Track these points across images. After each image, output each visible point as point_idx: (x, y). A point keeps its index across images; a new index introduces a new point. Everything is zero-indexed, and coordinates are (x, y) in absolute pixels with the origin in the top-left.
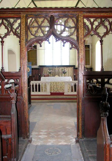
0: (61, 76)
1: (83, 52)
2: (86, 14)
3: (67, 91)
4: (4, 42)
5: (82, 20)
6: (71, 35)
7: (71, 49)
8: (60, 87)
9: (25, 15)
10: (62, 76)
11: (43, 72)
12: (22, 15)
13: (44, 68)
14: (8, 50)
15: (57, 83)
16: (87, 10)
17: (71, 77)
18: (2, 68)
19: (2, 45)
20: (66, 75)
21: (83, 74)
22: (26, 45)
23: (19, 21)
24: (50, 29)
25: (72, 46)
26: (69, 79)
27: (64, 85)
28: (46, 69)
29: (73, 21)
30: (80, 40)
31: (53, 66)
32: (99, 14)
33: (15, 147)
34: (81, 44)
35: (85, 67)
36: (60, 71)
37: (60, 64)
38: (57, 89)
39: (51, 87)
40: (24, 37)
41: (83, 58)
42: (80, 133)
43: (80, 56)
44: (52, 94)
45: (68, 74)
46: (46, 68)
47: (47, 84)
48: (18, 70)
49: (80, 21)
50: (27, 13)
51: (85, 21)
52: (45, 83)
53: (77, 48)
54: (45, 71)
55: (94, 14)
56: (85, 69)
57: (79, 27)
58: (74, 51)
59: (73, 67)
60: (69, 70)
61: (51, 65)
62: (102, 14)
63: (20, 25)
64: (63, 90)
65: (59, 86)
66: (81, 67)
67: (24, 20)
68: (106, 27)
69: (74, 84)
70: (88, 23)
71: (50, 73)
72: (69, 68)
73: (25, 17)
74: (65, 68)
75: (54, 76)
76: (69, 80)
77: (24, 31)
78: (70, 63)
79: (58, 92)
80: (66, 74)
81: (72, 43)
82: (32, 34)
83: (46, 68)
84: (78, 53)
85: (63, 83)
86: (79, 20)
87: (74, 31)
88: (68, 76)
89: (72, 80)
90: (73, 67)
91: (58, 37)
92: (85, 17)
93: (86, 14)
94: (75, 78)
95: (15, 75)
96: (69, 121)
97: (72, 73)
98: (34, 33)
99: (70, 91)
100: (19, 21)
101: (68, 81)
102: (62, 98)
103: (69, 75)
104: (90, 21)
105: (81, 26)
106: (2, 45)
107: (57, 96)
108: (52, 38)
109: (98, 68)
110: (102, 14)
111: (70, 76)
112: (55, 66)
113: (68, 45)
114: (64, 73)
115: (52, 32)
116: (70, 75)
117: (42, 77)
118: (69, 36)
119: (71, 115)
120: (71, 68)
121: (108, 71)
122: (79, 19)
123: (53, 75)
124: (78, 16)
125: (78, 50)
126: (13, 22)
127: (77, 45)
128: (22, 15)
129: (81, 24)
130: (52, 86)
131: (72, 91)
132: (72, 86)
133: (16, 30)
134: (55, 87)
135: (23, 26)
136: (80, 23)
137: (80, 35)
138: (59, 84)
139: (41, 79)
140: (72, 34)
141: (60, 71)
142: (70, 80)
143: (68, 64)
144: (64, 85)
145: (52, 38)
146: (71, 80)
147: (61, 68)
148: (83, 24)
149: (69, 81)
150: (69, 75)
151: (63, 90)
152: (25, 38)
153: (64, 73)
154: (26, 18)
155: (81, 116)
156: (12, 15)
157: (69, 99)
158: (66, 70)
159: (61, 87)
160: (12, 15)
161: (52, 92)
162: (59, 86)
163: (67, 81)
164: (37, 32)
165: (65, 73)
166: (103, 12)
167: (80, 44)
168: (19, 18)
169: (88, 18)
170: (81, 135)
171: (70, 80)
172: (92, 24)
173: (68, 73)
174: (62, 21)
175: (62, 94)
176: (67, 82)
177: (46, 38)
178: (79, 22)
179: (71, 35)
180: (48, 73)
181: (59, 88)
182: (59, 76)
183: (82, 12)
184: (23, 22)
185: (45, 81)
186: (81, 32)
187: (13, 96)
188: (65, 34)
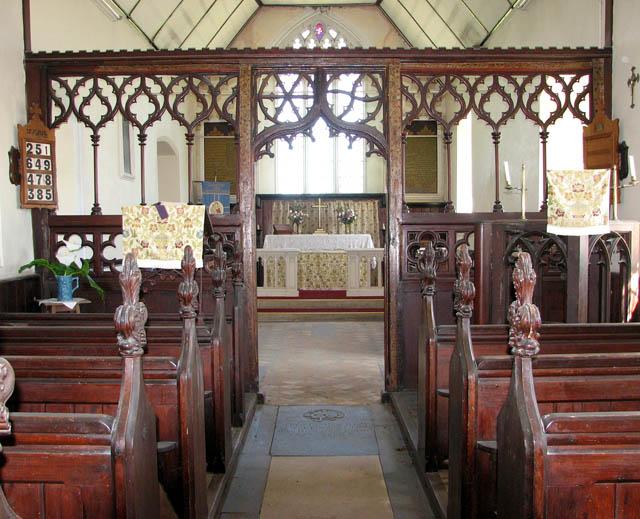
0: (334, 231)
1: (399, 165)
2: (407, 66)
3: (358, 286)
4: (99, 137)
5: (399, 80)
6: (368, 119)
7: (368, 155)
8: (330, 270)
9: (250, 68)
10: (338, 233)
11: (270, 217)
12: (242, 67)
13: (274, 205)
14: (158, 143)
15: (321, 256)
16: (411, 55)
17: (370, 236)
18: (96, 205)
19: (95, 146)
20: (352, 230)
21: (401, 220)
22: (252, 144)
23: (233, 83)
24: (314, 102)
25: (372, 147)
26: (364, 241)
27: (345, 265)
28: (281, 208)
29: (375, 81)
30: (391, 133)
31: (305, 197)
32: (441, 66)
33: (240, 384)
34: (396, 142)
35: (404, 203)
36: (333, 214)
37: (330, 191)
38: (321, 277)
39: (300, 272)
40: (249, 123)
41: (400, 180)
42: (393, 376)
43: (393, 173)
44: (303, 294)
45: (359, 225)
46: (281, 205)
47: (287, 260)
48: (89, 213)
49: (394, 83)
50: (254, 61)
51: (407, 82)
52: (281, 258)
53: (384, 152)
54: (281, 214)
55: (429, 66)
56: (404, 209)
57: (391, 99)
58: (377, 161)
59: (376, 202)
60: (362, 211)
61: (300, 191)
62: (450, 66)
63: (236, 93)
64: (341, 280)
65: (328, 268)
66: (396, 202)
67: (246, 80)
68: (555, 97)
69: (380, 260)
70: (413, 90)
71: (296, 221)
72: (364, 203)
73: (250, 73)
74: (350, 202)
75: (309, 233)
76: (364, 245)
77: (249, 108)
78: (366, 185)
79: (323, 289)
80: (352, 225)
81: (371, 141)
82: (267, 117)
83: (281, 205)
84: (388, 166)
85: (341, 255)
86: (390, 80)
87: (378, 109)
88: (362, 233)
89: (376, 246)
90: (376, 202)
91: (336, 126)
92: (404, 72)
93: (407, 66)
94: (383, 238)
95: (224, 223)
96: (364, 363)
97: (375, 221)
98: (271, 113)
99: (368, 283)
100: (233, 83)
101: (360, 249)
102: (340, 306)
103: (362, 229)
104: (564, 83)
105: (394, 97)
106: (95, 146)
107: (321, 301)
108: (320, 127)
109: (465, 204)
110: (450, 66)
111: (368, 232)
112: (315, 198)
113: (360, 144)
114: (347, 220)
115: (321, 109)
116: (366, 229)
117: (267, 236)
118: (363, 122)
119: (367, 349)
120: (370, 204)
121: (83, 214)
122: (391, 77)
123: (307, 230)
124: (388, 68)
125: (387, 158)
126: (218, 86)
127: (385, 145)
128: (242, 67)
129: (394, 91)
130: (304, 269)
131: (374, 283)
132: (374, 267)
133: (225, 107)
134: (314, 268)
135: (245, 96)
136: (391, 90)
137: (392, 120)
138: (330, 259)
139: (266, 241)
140: (371, 117)
141: (333, 214)
142: (366, 246)
143: (360, 190)
144: (345, 265)
145: (320, 127)
146: (371, 246)
147: (334, 205)
148: (399, 91)
149: (363, 249)
150: (362, 229)
151: (341, 280)
152: (249, 128)
153: (347, 220)
154: (252, 73)
155: (394, 330)
156: (215, 67)
157: (361, 311)
158: (354, 209)
159: (334, 272)
160: (215, 67)
161: (304, 289)
162: (328, 268)
163: (356, 248)
164: (278, 110)
165: (350, 221)
166: (452, 60)
167: (391, 142)
168: (236, 74)
169: (412, 74)
170: (395, 382)
171: (366, 246)
172: (568, 90)
173: (359, 221)
174: (339, 33)
175: (342, 294)
176: (358, 253)
177: (305, 126)
178: (390, 84)
179: (368, 119)
180: (288, 222)
181: (328, 276)
182: (328, 232)
183: (398, 61)
184: (245, 84)
185: (279, 249)
186: (395, 112)
187: (191, 291)
188: (352, 118)
